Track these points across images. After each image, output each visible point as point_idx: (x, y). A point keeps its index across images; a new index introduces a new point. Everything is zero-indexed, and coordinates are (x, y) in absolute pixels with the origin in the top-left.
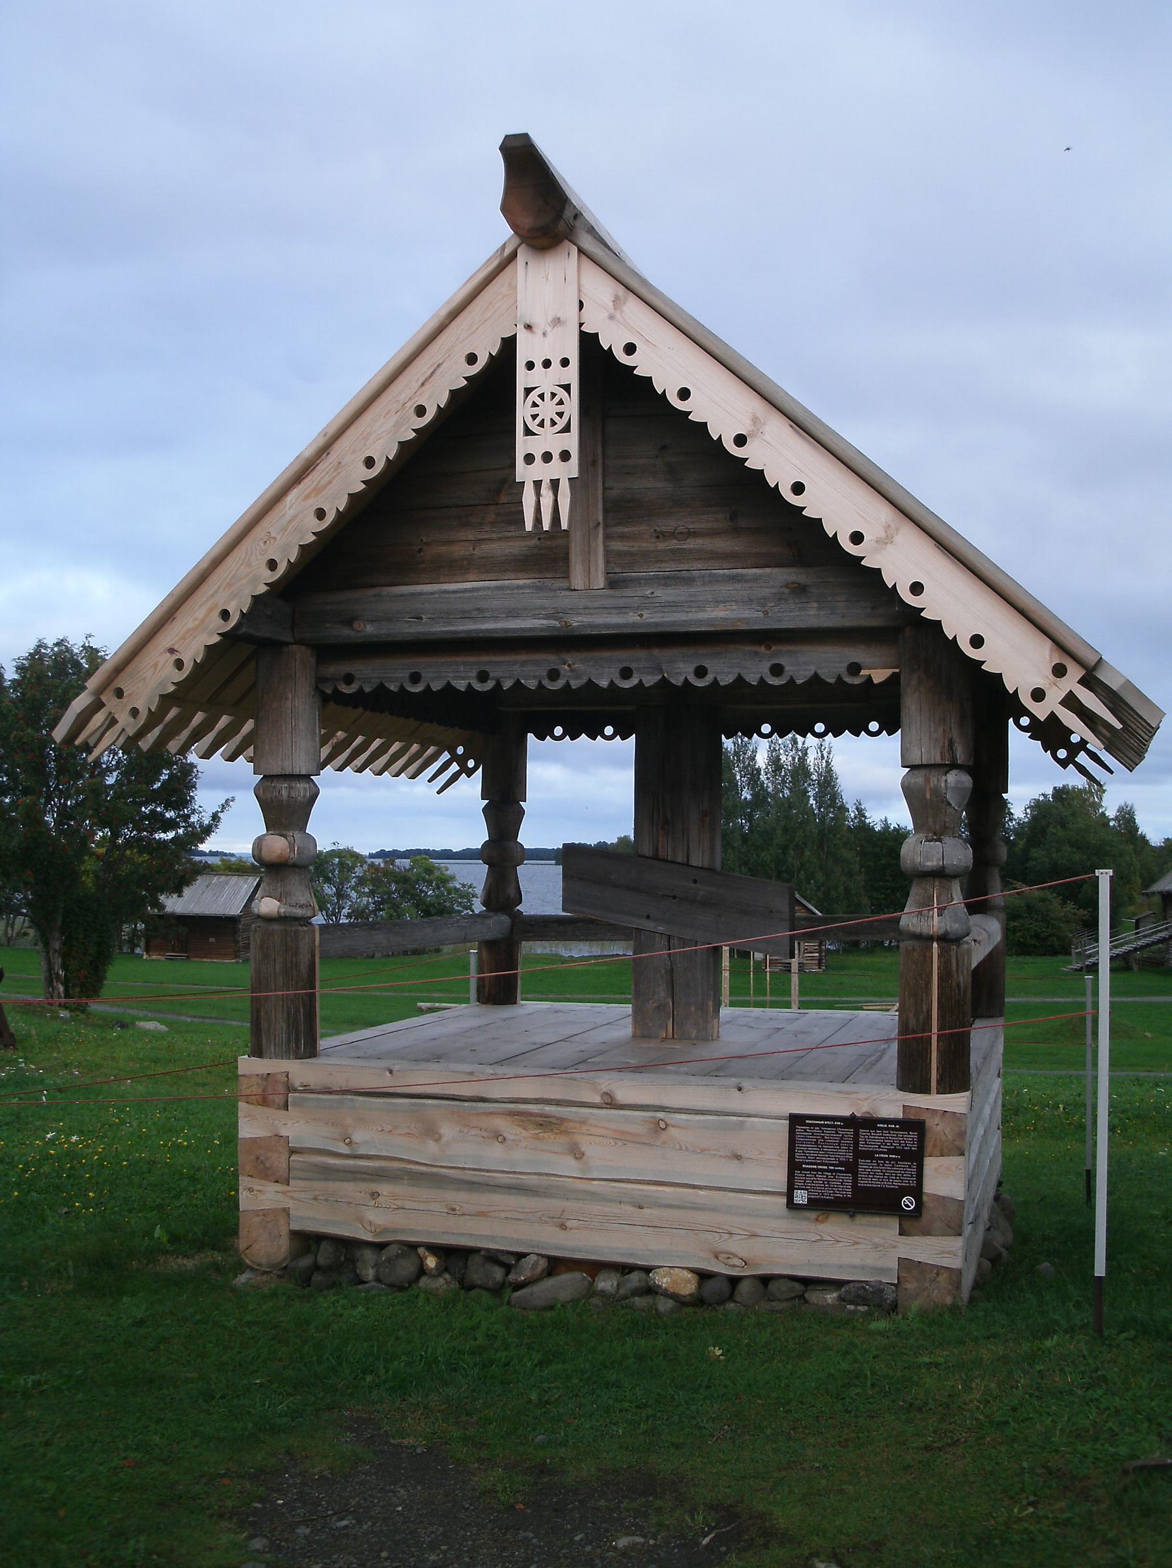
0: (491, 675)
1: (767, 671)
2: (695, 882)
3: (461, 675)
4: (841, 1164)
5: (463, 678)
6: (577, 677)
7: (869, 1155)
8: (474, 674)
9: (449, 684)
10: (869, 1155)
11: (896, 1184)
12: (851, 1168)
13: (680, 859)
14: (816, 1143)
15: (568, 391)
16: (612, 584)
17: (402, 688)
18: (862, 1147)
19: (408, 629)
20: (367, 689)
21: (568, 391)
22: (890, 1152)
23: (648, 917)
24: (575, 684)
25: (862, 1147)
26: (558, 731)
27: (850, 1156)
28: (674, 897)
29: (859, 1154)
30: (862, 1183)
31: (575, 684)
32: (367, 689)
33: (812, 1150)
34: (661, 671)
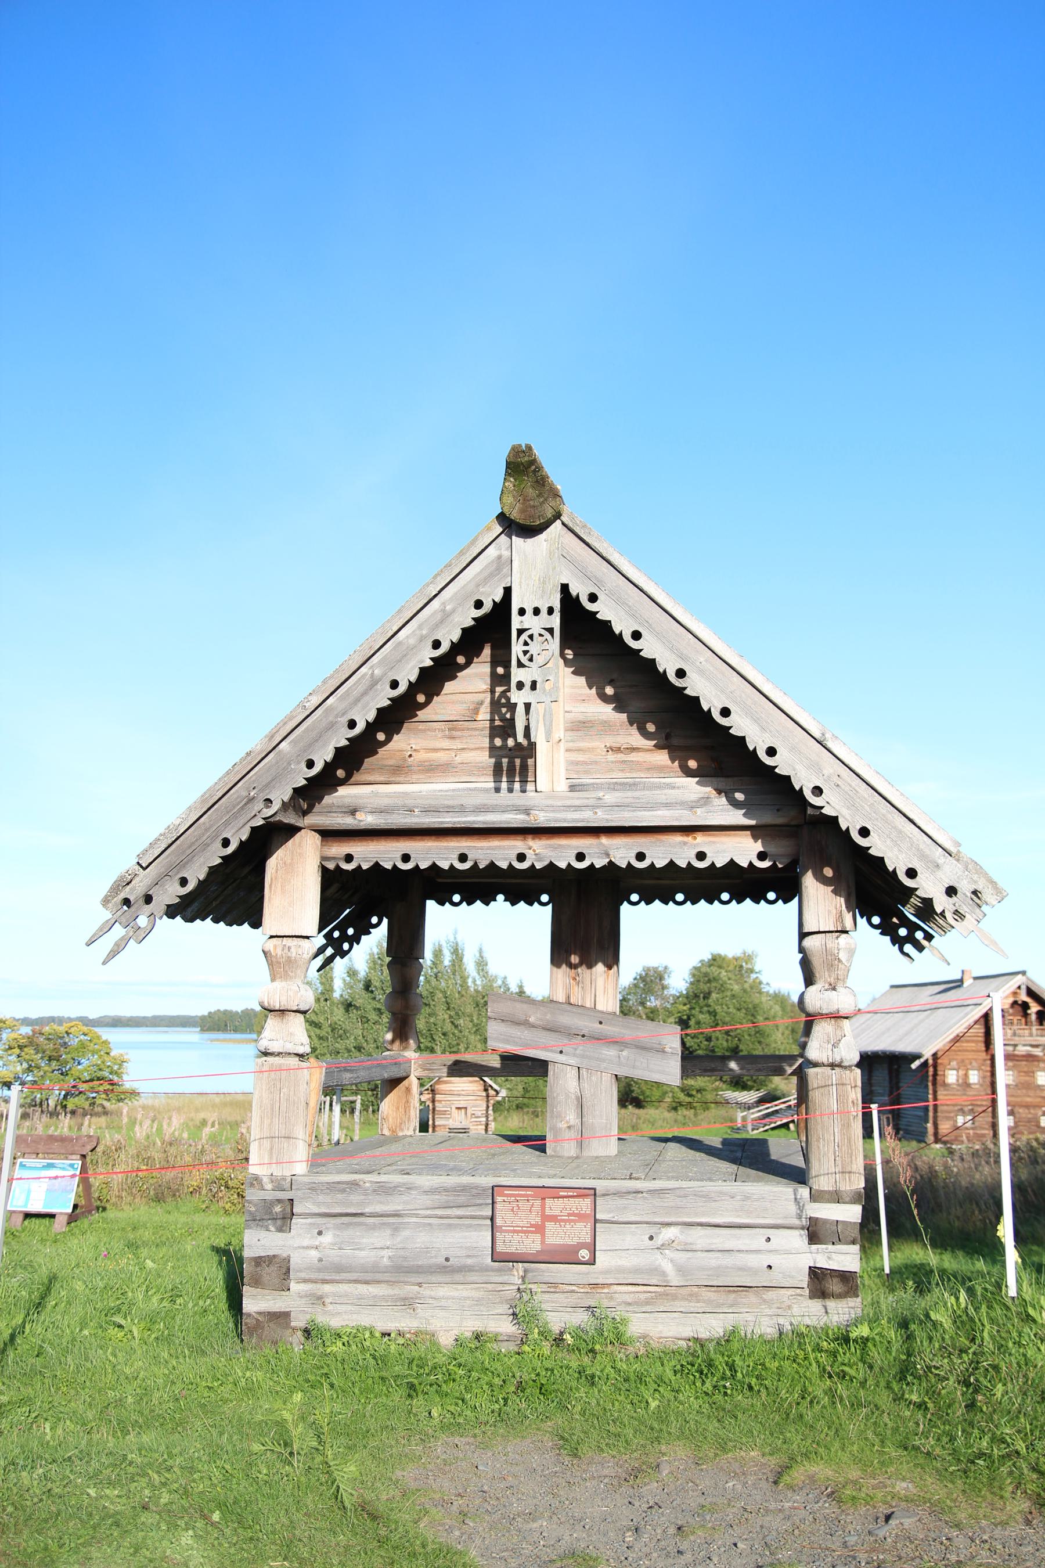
0: (469, 857)
1: (694, 856)
2: (601, 1023)
3: (562, 854)
4: (532, 1226)
5: (446, 859)
6: (540, 860)
7: (554, 1219)
8: (456, 856)
9: (434, 864)
10: (554, 1219)
11: (575, 1241)
12: (540, 1229)
13: (588, 1005)
14: (512, 1210)
15: (519, 661)
16: (573, 788)
17: (338, 866)
18: (548, 1212)
19: (367, 820)
20: (365, 867)
21: (519, 661)
22: (569, 1215)
23: (561, 1052)
24: (538, 866)
25: (548, 1212)
26: (456, 898)
27: (538, 1220)
28: (583, 1036)
29: (546, 1218)
30: (548, 1241)
31: (538, 866)
32: (365, 867)
33: (509, 1216)
34: (608, 855)
